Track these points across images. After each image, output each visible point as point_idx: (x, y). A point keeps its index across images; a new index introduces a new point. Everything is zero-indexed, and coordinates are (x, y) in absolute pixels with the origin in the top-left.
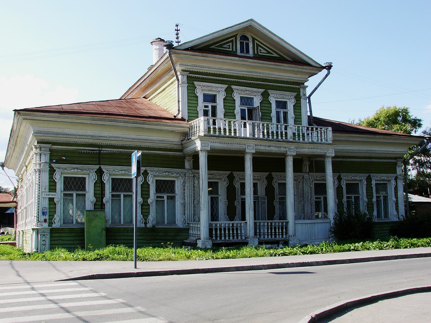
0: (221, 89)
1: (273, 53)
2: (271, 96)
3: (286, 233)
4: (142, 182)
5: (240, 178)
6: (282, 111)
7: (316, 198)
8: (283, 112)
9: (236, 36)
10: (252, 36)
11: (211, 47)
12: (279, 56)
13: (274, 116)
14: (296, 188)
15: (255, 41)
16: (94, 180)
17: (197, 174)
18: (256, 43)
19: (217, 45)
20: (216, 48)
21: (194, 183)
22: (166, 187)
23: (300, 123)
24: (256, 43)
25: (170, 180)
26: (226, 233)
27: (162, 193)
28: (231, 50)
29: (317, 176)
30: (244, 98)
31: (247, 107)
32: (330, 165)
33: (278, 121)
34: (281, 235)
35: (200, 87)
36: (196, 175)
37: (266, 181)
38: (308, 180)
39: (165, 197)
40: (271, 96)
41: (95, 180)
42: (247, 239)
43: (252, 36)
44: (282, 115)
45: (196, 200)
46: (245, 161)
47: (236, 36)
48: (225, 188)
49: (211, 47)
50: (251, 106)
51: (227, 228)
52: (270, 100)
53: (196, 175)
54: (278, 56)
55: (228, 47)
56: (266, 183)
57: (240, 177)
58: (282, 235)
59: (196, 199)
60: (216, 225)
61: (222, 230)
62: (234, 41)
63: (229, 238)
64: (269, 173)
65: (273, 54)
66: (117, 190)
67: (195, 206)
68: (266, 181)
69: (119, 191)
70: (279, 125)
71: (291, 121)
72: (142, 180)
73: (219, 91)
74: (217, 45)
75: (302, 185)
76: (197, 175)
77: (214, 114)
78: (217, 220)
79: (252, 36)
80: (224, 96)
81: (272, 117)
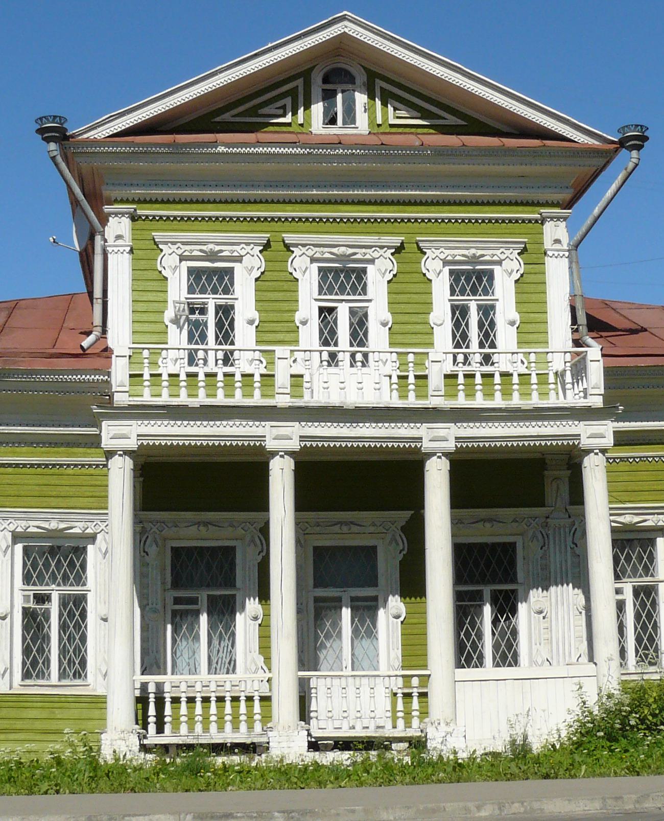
0: (248, 248)
1: (442, 115)
2: (428, 258)
3: (424, 713)
4: (402, 555)
5: (306, 532)
6: (212, 302)
7: (177, 601)
8: (480, 307)
9: (306, 75)
10: (364, 68)
11: (218, 119)
12: (466, 124)
13: (439, 323)
14: (524, 559)
15: (375, 81)
16: (400, 553)
17: (534, 520)
18: (381, 88)
19: (241, 109)
20: (238, 119)
21: (142, 553)
22: (47, 565)
23: (540, 337)
24: (381, 88)
25: (196, 548)
26: (149, 714)
27: (221, 585)
28: (290, 121)
29: (459, 520)
30: (221, 272)
31: (476, 300)
32: (595, 477)
33: (460, 338)
34: (260, 724)
35: (174, 247)
36: (151, 529)
37: (260, 540)
38: (567, 530)
39: (487, 594)
40: (428, 258)
41: (261, 554)
42: (270, 734)
43: (364, 68)
44: (474, 317)
45: (150, 606)
46: (583, 469)
47: (306, 75)
48: (254, 565)
49: (218, 119)
50: (360, 294)
51: (152, 696)
52: (424, 271)
53: (532, 521)
54: (265, 129)
55: (281, 112)
56: (403, 543)
57: (305, 530)
58: (408, 715)
59: (150, 604)
60: (159, 686)
61: (164, 703)
62: (301, 90)
63: (189, 729)
64: (413, 512)
65: (233, 116)
66: (41, 579)
67: (148, 625)
68: (260, 540)
69: (478, 583)
70: (326, 352)
71: (506, 337)
72: (401, 548)
73: (242, 256)
74: (241, 109)
75: (541, 549)
76: (154, 529)
77: (225, 331)
78: (161, 670)
79: (366, 66)
80: (258, 269)
81: (433, 325)
